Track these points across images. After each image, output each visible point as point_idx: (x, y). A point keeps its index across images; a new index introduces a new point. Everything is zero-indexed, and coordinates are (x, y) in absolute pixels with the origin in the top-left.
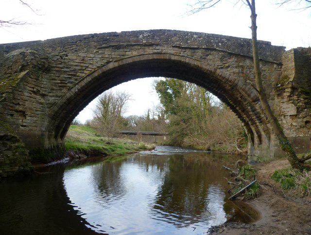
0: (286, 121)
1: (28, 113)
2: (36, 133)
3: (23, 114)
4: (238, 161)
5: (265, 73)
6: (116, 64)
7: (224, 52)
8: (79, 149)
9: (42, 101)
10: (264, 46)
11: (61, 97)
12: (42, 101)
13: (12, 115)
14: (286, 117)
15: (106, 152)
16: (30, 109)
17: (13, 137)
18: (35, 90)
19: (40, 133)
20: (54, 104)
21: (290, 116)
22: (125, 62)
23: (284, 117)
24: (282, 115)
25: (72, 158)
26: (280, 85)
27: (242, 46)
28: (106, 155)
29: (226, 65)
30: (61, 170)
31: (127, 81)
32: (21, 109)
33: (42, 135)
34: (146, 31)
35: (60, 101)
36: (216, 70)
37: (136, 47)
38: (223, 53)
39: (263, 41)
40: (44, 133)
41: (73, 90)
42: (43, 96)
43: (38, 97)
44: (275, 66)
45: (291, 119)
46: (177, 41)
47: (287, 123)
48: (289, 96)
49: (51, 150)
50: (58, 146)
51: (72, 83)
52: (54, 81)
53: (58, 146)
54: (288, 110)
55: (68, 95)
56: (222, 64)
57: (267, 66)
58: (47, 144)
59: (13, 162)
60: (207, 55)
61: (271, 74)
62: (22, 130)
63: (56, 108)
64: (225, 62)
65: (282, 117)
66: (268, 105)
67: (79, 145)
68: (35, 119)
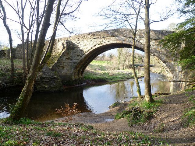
1: (65, 67)
2: (69, 74)
3: (63, 67)
6: (99, 46)
8: (92, 79)
9: (71, 61)
11: (78, 60)
12: (71, 61)
13: (59, 68)
15: (107, 80)
16: (66, 65)
17: (57, 78)
18: (68, 58)
19: (70, 74)
20: (75, 63)
22: (102, 45)
25: (88, 83)
28: (106, 81)
30: (82, 89)
32: (62, 66)
33: (71, 75)
34: (111, 30)
35: (78, 62)
37: (107, 38)
39: (171, 31)
40: (72, 74)
41: (82, 57)
42: (71, 59)
43: (69, 60)
46: (125, 34)
49: (75, 81)
50: (79, 79)
51: (82, 54)
52: (75, 53)
53: (79, 79)
55: (80, 59)
58: (73, 78)
59: (56, 87)
62: (22, 97)
63: (76, 64)
67: (93, 77)
68: (68, 69)
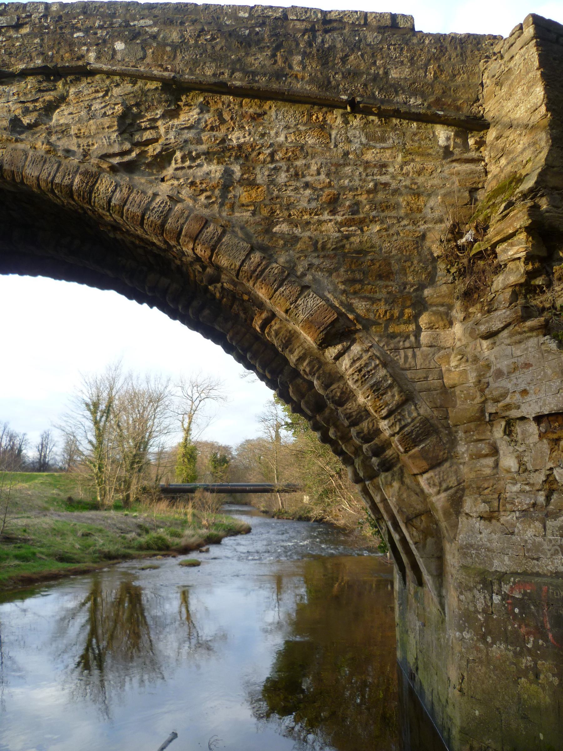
0: (519, 459)
4: (176, 530)
5: (384, 179)
7: (134, 78)
10: (372, 37)
14: (518, 428)
21: (538, 419)
23: (508, 431)
24: (494, 416)
26: (468, 237)
27: (249, 43)
29: (150, 148)
31: (81, 282)
36: (92, 177)
38: (128, 87)
39: (365, 15)
44: (443, 135)
45: (545, 445)
47: (523, 468)
48: (525, 289)
54: (522, 380)
56: (127, 146)
57: (392, 138)
60: (50, 108)
61: (422, 173)
64: (147, 135)
65: (498, 432)
66: (550, 415)
